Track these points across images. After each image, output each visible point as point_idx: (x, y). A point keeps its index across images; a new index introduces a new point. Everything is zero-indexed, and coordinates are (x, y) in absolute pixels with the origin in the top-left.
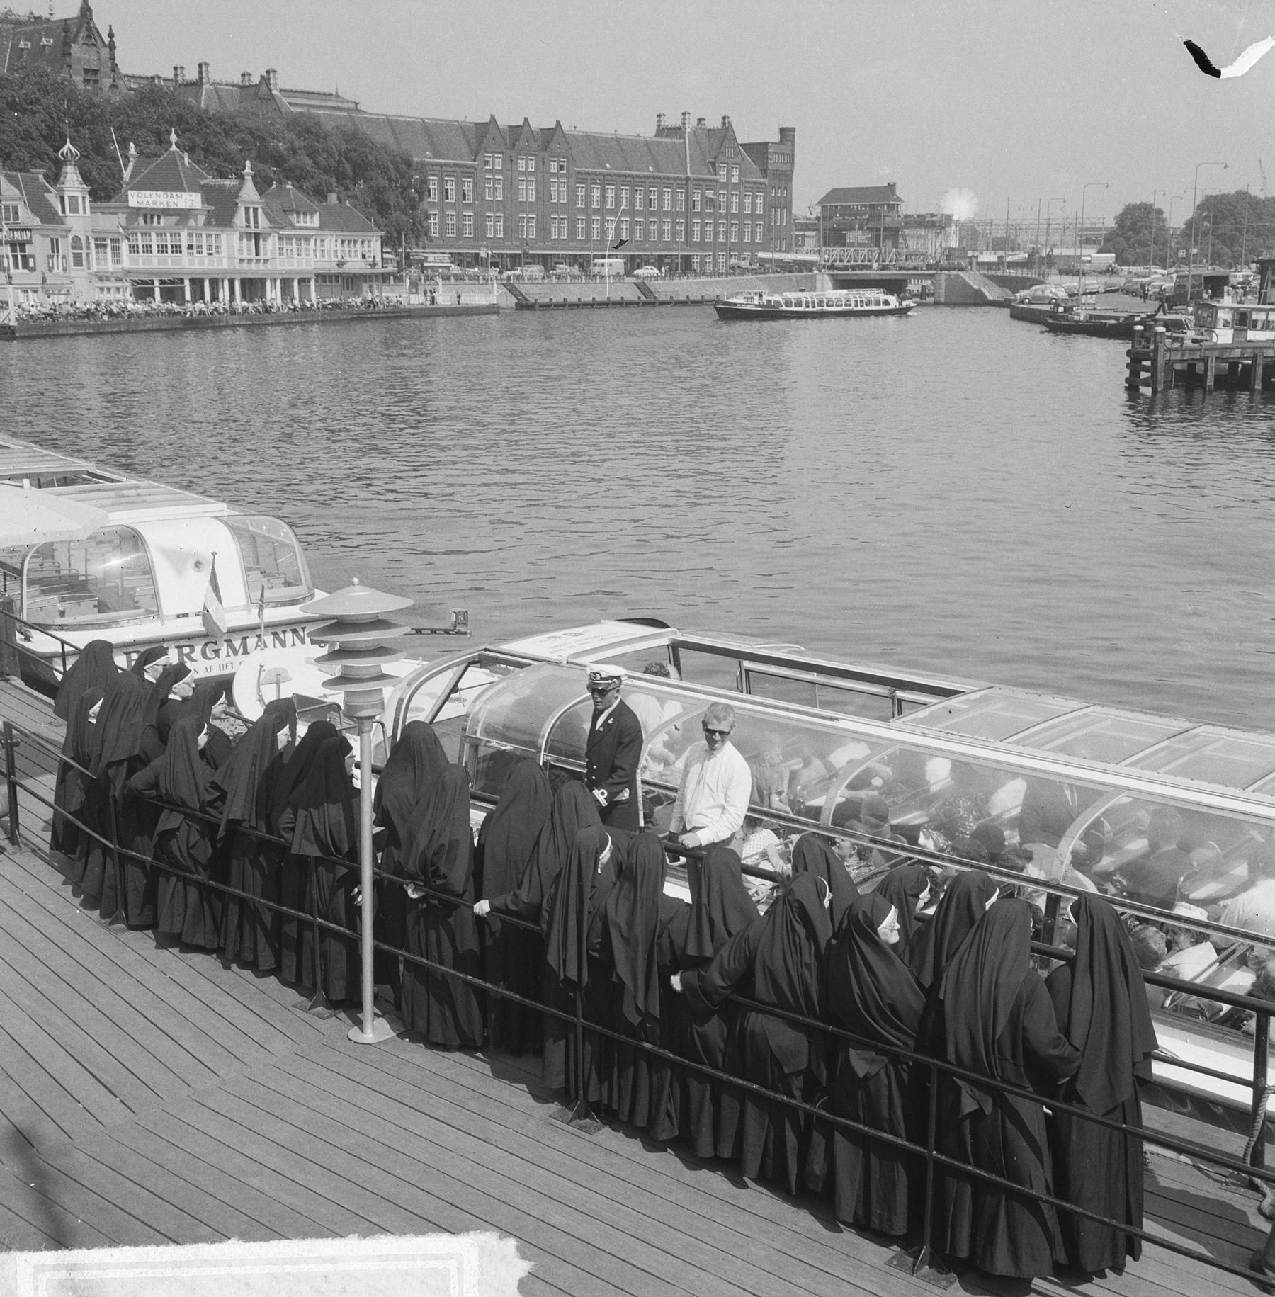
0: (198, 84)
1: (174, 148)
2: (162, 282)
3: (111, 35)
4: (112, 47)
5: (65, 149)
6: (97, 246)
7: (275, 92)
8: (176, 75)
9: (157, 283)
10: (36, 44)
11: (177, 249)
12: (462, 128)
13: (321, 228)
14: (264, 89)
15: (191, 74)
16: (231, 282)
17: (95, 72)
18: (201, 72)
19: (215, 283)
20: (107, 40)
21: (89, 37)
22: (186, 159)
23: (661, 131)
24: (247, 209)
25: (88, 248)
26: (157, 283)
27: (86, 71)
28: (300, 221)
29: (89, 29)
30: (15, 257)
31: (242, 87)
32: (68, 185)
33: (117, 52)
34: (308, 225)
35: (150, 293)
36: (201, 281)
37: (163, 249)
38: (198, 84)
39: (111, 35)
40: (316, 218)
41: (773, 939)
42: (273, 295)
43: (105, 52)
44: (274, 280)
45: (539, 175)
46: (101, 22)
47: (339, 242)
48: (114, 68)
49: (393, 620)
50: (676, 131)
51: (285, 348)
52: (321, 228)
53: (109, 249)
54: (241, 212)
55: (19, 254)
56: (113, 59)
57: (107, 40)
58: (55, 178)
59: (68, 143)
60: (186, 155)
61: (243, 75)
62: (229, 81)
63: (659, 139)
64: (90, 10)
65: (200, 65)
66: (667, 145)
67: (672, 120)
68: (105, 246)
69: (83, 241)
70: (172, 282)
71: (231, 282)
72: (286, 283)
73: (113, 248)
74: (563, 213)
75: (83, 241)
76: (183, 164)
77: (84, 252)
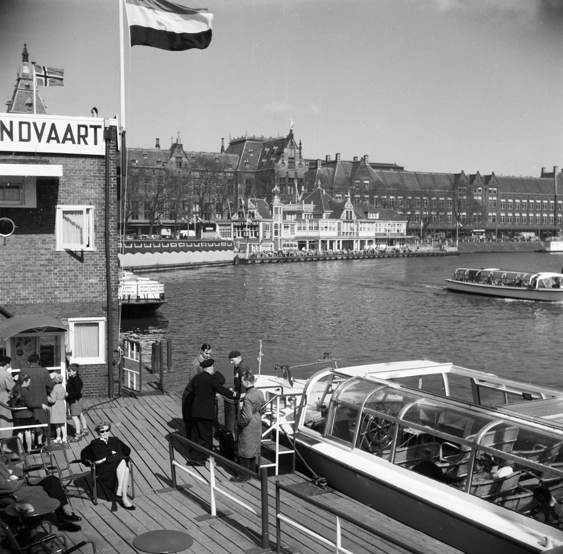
0: (335, 162)
1: (319, 187)
2: (310, 242)
3: (300, 144)
4: (300, 149)
5: (275, 189)
6: (285, 227)
7: (367, 164)
8: (327, 159)
9: (308, 242)
10: (446, 200)
11: (317, 228)
12: (448, 176)
13: (380, 219)
14: (362, 163)
15: (333, 158)
16: (339, 242)
17: (293, 158)
18: (337, 157)
19: (331, 243)
20: (298, 146)
21: (292, 145)
22: (324, 192)
23: (544, 175)
24: (347, 212)
25: (281, 228)
26: (308, 242)
27: (289, 158)
28: (371, 216)
29: (292, 142)
30: (252, 232)
31: (353, 163)
32: (275, 203)
33: (302, 151)
34: (374, 218)
35: (304, 245)
36: (326, 242)
37: (311, 228)
38: (335, 162)
39: (300, 144)
40: (378, 215)
41: (557, 489)
42: (356, 246)
43: (297, 151)
44: (357, 241)
45: (484, 196)
46: (296, 139)
47: (387, 225)
48: (301, 157)
49: (445, 292)
50: (552, 175)
51: (432, 236)
52: (380, 219)
53: (289, 228)
54: (345, 212)
55: (253, 231)
56: (300, 153)
57: (298, 146)
58: (270, 200)
59: (276, 187)
60: (324, 190)
61: (354, 158)
62: (348, 160)
63: (542, 179)
64: (293, 135)
65: (337, 155)
66: (546, 181)
67: (549, 170)
68: (288, 227)
69: (279, 226)
70: (314, 242)
71: (339, 242)
72: (362, 243)
73: (291, 228)
74: (494, 212)
75: (279, 226)
76: (323, 194)
77: (279, 230)
